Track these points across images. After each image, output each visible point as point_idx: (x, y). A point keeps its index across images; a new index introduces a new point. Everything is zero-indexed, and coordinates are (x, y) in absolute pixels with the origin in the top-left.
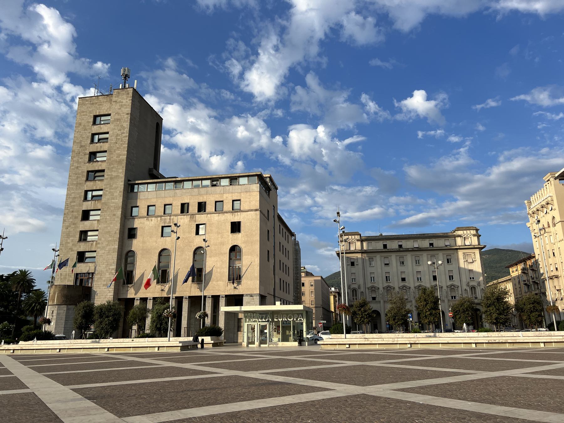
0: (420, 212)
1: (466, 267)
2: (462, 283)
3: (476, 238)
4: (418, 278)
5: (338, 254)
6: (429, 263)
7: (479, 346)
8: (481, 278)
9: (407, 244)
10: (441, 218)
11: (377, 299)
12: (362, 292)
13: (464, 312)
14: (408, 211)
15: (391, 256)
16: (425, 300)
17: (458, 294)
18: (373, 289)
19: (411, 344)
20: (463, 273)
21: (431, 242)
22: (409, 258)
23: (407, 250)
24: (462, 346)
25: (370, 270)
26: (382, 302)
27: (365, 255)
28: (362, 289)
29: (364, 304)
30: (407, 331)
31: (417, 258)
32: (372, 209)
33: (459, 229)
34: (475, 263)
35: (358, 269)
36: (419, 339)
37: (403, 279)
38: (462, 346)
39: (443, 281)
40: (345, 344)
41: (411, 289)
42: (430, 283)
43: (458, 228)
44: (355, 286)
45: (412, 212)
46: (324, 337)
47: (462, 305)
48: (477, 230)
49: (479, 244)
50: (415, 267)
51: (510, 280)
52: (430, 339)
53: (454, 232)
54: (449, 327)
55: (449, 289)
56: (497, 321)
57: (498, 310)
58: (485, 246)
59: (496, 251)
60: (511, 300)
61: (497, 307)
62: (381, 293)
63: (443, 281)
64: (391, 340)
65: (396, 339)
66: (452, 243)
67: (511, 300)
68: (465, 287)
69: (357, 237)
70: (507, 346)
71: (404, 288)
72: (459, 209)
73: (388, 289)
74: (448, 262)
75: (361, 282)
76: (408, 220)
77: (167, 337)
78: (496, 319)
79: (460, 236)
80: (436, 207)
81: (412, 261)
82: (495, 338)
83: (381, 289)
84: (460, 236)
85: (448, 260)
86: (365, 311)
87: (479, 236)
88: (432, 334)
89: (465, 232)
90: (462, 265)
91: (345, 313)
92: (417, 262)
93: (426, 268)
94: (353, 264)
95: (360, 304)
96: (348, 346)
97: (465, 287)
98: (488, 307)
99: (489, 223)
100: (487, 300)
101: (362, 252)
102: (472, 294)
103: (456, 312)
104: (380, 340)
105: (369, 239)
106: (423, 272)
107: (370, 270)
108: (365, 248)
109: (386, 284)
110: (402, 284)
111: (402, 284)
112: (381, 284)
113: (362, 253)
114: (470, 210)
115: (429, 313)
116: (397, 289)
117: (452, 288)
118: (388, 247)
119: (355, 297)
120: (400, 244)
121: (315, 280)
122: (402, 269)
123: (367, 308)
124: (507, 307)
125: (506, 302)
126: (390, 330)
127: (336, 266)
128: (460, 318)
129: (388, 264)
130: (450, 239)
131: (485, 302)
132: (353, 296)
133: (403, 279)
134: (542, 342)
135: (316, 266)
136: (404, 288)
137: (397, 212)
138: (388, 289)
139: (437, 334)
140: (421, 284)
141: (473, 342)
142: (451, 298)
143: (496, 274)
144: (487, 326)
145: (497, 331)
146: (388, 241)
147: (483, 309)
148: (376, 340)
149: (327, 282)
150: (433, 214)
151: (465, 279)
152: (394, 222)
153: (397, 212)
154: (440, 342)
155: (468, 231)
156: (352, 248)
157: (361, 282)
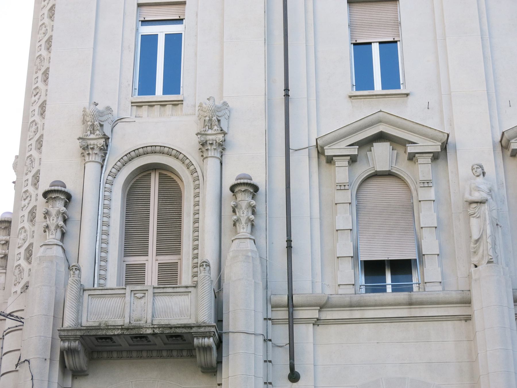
11: (429, 276)
44: (170, 130)
119: (151, 263)
132: (133, 239)
140: (392, 108)
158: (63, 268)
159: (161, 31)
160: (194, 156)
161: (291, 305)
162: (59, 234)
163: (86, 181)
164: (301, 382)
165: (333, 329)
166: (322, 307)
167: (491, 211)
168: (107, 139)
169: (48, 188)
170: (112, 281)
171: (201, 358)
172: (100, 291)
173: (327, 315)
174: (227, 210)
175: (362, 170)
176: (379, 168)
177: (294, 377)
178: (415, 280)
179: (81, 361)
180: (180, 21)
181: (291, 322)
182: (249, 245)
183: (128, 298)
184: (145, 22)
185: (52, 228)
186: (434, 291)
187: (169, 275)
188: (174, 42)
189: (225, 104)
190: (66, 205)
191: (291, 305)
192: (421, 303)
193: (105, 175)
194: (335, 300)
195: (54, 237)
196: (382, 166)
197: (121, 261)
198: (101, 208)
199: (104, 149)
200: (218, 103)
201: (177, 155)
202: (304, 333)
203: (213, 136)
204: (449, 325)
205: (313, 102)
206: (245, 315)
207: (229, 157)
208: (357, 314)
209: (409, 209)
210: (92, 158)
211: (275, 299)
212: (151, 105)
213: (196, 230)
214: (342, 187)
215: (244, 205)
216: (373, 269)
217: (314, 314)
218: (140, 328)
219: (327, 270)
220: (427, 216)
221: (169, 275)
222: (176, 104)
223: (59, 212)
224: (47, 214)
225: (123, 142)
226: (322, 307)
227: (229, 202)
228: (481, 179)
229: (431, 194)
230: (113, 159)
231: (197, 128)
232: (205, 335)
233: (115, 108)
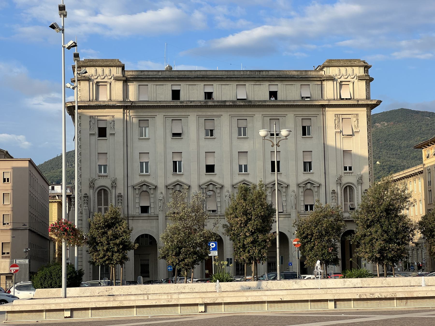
0: (259, 22)
1: (338, 146)
2: (326, 176)
3: (363, 83)
4: (240, 166)
5: (71, 110)
6: (263, 133)
7: (342, 306)
8: (366, 169)
9: (223, 92)
10: (301, 39)
11: (151, 211)
12: (120, 196)
13: (321, 236)
14: (234, 19)
15: (187, 116)
16: (245, 213)
17: (322, 200)
18: (145, 189)
19: (206, 305)
20: (331, 155)
21: (273, 89)
22: (225, 122)
23: (223, 105)
24: (309, 307)
25: (139, 146)
26: (161, 217)
27: (131, 113)
28: (120, 189)
29: (112, 223)
30: (207, 278)
31: (242, 124)
32: (155, 9)
33: (330, 64)
34: (357, 137)
35: (112, 145)
36: (225, 294)
37: (210, 169)
38: (309, 307)
39: (292, 174)
40: (63, 310)
41: (225, 190)
42: (199, 178)
43: (330, 61)
44: (106, 183)
45: (242, 22)
46: (22, 294)
47: (318, 222)
48: (367, 67)
49: (368, 98)
50: (236, 142)
51: (421, 172)
52: (247, 294)
53: (322, 69)
54: (296, 268)
55: (301, 190)
56: (382, 255)
57: (386, 232)
58: (379, 102)
59: (404, 115)
60: (415, 212)
61: (385, 228)
62: (160, 197)
63: (292, 174)
64: (165, 297)
65: (175, 296)
66: (316, 94)
67: (415, 212)
68: (333, 186)
69: (116, 72)
70: (395, 305)
71: (211, 189)
72: (339, 22)
73: (177, 188)
74: (304, 134)
75: (119, 174)
76: (232, 40)
77: (60, 287)
78: (381, 251)
79: (331, 79)
80: (293, 13)
81: (198, 130)
82: (373, 290)
84: (331, 79)
85: (304, 128)
86: (116, 237)
87: (369, 80)
88: (254, 284)
89: (343, 69)
90: (331, 141)
91: (67, 240)
92: (242, 132)
93: (258, 145)
94: (102, 132)
95: (106, 221)
96: (68, 314)
97: (333, 186)
98: (369, 226)
99: (396, 54)
100: (368, 212)
101: (126, 106)
102: (346, 200)
103: (306, 237)
104: (141, 297)
105: (143, 78)
106: (239, 154)
107: (143, 146)
108: (132, 97)
109: (172, 179)
110: (206, 178)
111: (206, 178)
112: (161, 176)
113: (125, 108)
114: (360, 24)
115: (250, 239)
116: (195, 190)
117: (308, 187)
118: (183, 96)
119: (103, 207)
120: (208, 90)
121: (14, 169)
122: (208, 145)
123: (120, 229)
124: (406, 229)
125: (403, 217)
126: (174, 275)
127: (61, 139)
128: (312, 249)
129: (179, 135)
130: (311, 84)
131: (363, 216)
132: (99, 204)
133: (210, 169)
134: (331, 300)
135: (21, 137)
136: (211, 187)
137: (210, 20)
138: (177, 188)
139: (264, 284)
141: (201, 302)
142: (303, 208)
143: (399, 161)
144: (367, 266)
145: (382, 275)
146: (182, 84)
147: (359, 231)
148: (133, 298)
149: (44, 175)
150: (285, 28)
151: (335, 170)
152: (201, 43)
153: (210, 20)
154: (265, 299)
155: (349, 69)
156: (104, 97)
157: (119, 174)
160: (110, 188)
161: (128, 217)
173: (134, 218)
187: (106, 209)
191: (128, 217)
198: (93, 196)
202: (130, 221)
204: (155, 220)
214: (137, 194)
220: (152, 200)
221: (106, 209)
227: (117, 199)
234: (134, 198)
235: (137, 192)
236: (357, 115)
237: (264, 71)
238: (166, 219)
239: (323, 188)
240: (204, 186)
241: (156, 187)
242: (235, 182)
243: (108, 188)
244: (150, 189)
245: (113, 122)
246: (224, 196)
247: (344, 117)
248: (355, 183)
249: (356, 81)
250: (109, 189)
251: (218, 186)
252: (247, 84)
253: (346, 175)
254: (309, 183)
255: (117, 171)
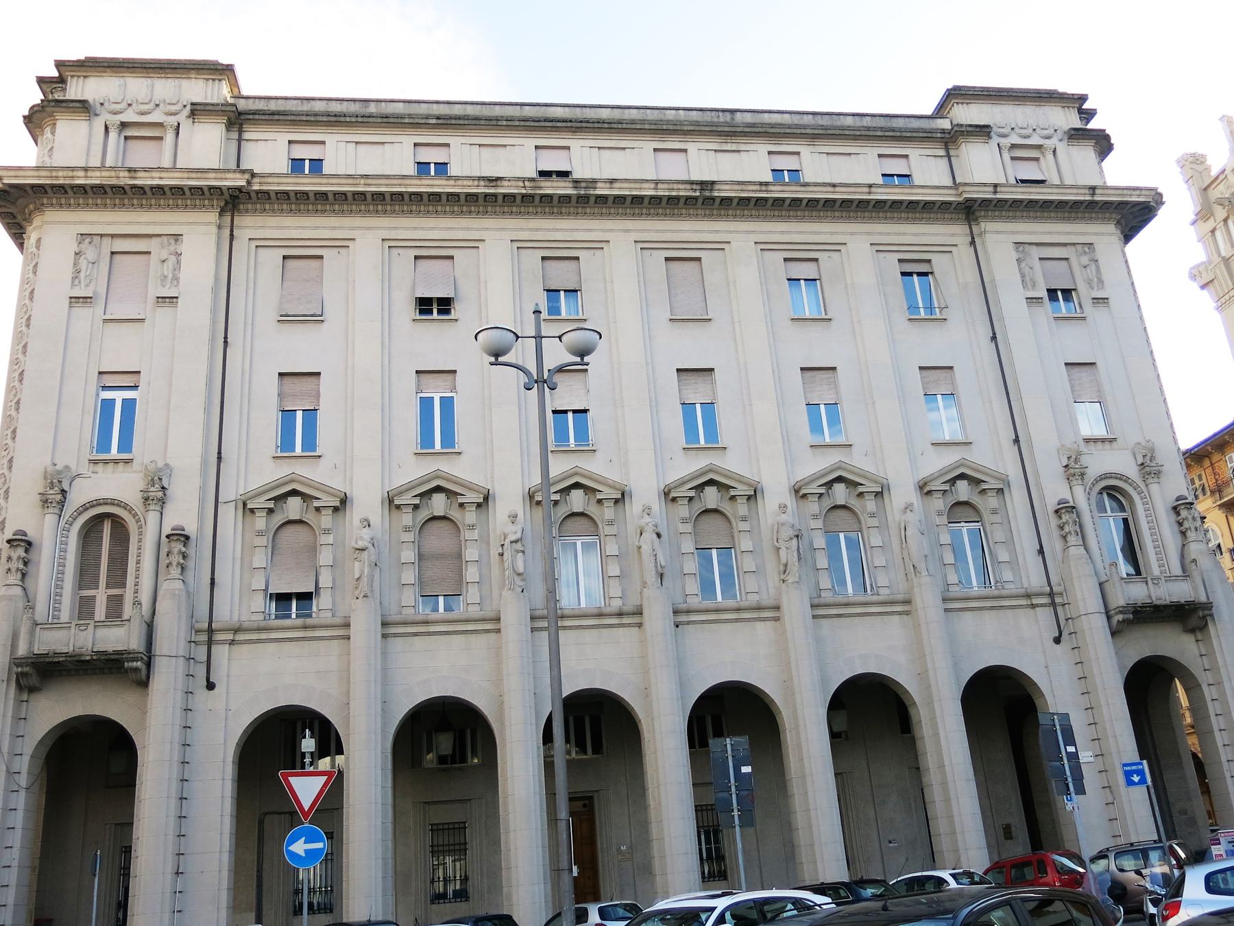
11: (322, 604)
18: (292, 510)
28: (184, 511)
44: (119, 486)
68: (1054, 489)
77: (586, 909)
79: (982, 131)
83: (776, 494)
112: (365, 458)
119: (101, 595)
129: (445, 305)
132: (86, 575)
140: (304, 470)
158: (21, 605)
159: (119, 396)
161: (210, 631)
162: (19, 575)
163: (44, 529)
164: (216, 690)
165: (245, 648)
166: (236, 631)
167: (369, 556)
168: (63, 492)
169: (11, 537)
170: (65, 616)
171: (133, 676)
172: (53, 624)
173: (241, 637)
174: (164, 550)
175: (278, 519)
176: (291, 518)
177: (211, 686)
178: (314, 609)
179: (34, 680)
180: (135, 387)
181: (210, 643)
182: (179, 584)
183: (73, 630)
184: (105, 388)
185: (13, 570)
186: (326, 617)
187: (115, 605)
188: (129, 405)
189: (167, 465)
190: (27, 551)
191: (210, 631)
192: (314, 627)
193: (62, 523)
194: (246, 625)
195: (14, 578)
196: (294, 516)
197: (74, 593)
199: (62, 503)
200: (160, 465)
201: (125, 506)
203: (155, 492)
205: (243, 462)
206: (172, 637)
207: (169, 508)
208: (264, 636)
209: (313, 549)
210: (51, 510)
211: (198, 626)
212: (106, 462)
213: (138, 570)
214: (260, 534)
215: (176, 551)
216: (282, 599)
217: (230, 637)
218: (81, 655)
219: (240, 601)
220: (325, 557)
221: (115, 605)
222: (128, 462)
223: (19, 558)
224: (9, 559)
225: (81, 494)
226: (236, 631)
228: (366, 530)
229: (330, 539)
230: (69, 509)
231: (141, 485)
232: (134, 660)
233: (73, 468)
234: (248, 549)
235: (260, 522)
236: (177, 237)
237: (867, 115)
238: (384, 636)
239: (1017, 498)
240: (814, 489)
241: (486, 498)
242: (673, 476)
243: (130, 510)
244: (318, 509)
245: (173, 259)
246: (631, 529)
247: (121, 245)
248: (1132, 472)
249: (1062, 148)
250: (135, 515)
251: (607, 493)
252: (692, 147)
253: (100, 467)
254: (577, 486)
255: (172, 434)
